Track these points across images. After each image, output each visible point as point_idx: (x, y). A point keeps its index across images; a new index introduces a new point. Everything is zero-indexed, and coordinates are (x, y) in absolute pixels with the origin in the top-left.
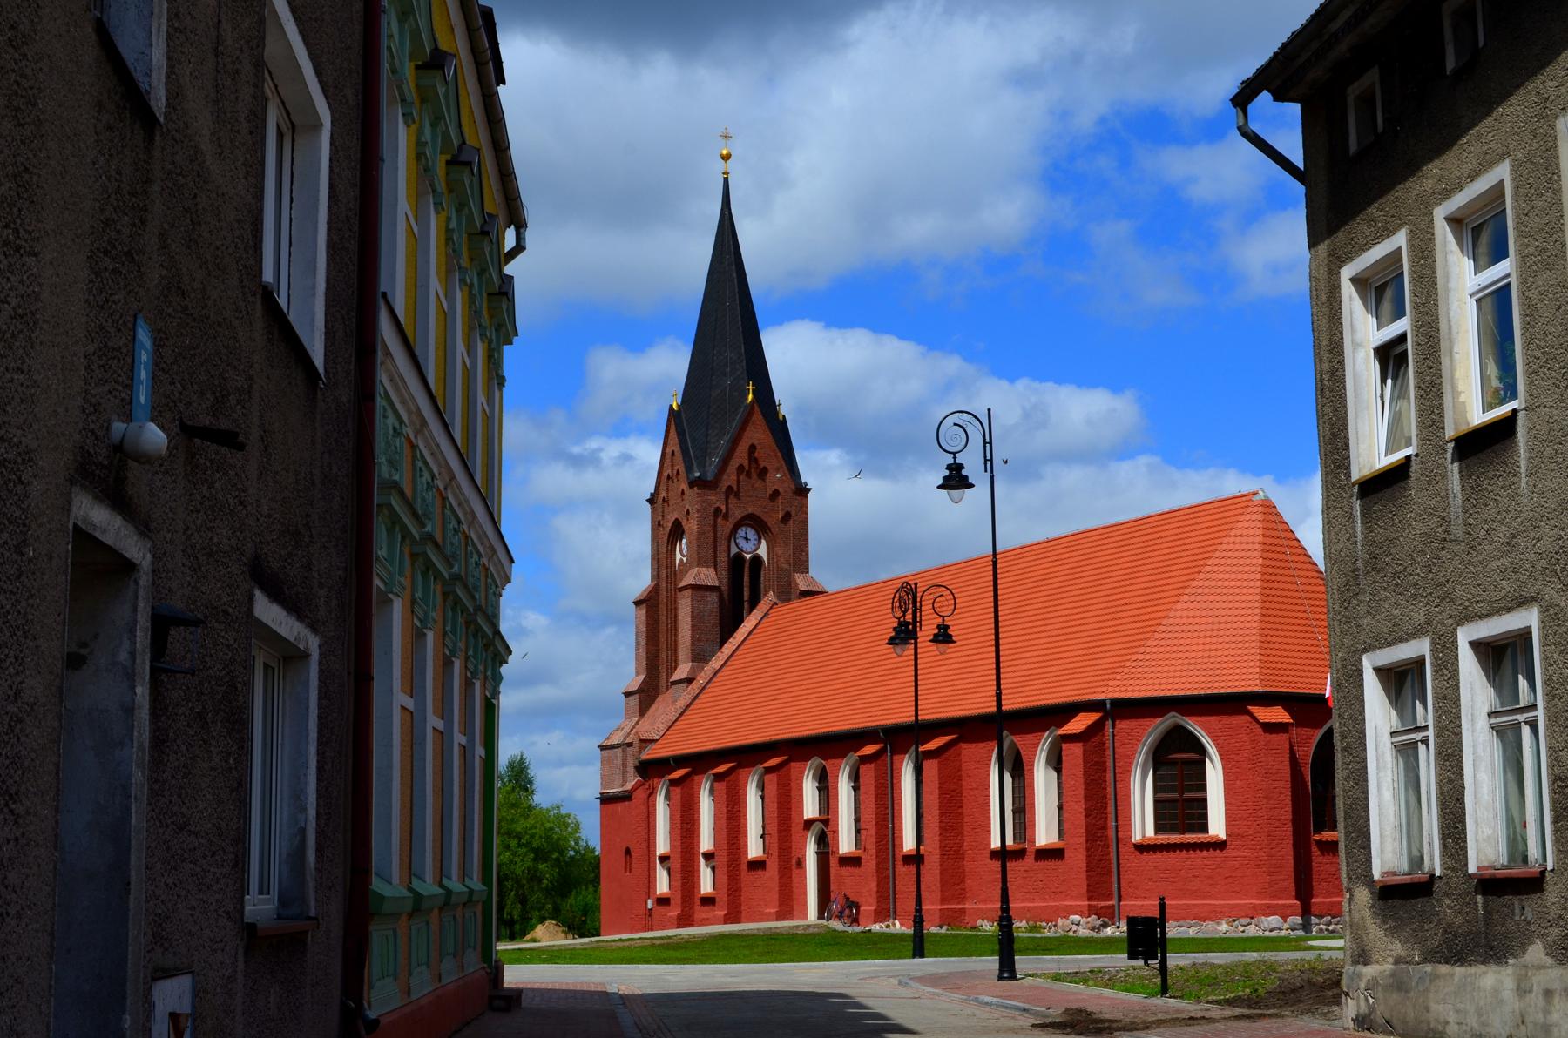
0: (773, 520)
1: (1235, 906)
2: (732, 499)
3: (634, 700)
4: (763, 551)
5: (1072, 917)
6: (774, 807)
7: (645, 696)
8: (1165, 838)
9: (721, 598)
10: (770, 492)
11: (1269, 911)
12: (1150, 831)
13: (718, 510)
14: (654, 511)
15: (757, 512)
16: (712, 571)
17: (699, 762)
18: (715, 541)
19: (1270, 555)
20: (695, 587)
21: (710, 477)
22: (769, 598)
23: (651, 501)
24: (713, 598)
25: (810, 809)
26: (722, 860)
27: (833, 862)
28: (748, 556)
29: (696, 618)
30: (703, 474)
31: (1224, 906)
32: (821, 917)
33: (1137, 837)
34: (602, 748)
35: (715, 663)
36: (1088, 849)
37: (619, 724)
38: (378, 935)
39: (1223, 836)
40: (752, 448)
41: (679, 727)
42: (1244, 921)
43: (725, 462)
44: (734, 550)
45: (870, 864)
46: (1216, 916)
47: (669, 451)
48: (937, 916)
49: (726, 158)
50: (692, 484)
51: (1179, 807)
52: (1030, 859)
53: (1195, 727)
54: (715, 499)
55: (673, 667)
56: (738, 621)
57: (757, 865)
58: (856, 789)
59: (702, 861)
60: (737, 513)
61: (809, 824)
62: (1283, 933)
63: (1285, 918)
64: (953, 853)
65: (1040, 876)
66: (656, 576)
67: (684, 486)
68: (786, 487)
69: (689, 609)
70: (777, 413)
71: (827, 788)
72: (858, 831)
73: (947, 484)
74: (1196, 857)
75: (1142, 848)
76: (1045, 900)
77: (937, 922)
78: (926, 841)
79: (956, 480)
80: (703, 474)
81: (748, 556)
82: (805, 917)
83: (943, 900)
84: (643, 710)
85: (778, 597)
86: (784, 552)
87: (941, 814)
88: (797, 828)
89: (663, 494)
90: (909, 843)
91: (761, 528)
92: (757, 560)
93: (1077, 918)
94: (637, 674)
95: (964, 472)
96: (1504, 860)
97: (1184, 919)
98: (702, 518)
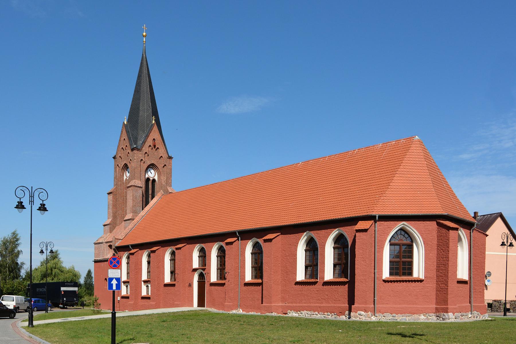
0: (160, 166)
2: (146, 157)
4: (156, 178)
6: (434, 254)
7: (111, 226)
14: (115, 162)
17: (142, 246)
25: (196, 264)
27: (207, 286)
28: (151, 179)
29: (134, 199)
32: (199, 305)
33: (384, 278)
34: (95, 244)
43: (144, 142)
44: (147, 176)
46: (418, 312)
51: (402, 265)
52: (319, 286)
53: (410, 226)
56: (147, 203)
60: (149, 163)
61: (195, 270)
65: (327, 293)
66: (116, 184)
67: (129, 151)
79: (20, 206)
81: (151, 179)
82: (192, 305)
86: (164, 178)
92: (154, 180)
94: (108, 218)
96: (304, 279)
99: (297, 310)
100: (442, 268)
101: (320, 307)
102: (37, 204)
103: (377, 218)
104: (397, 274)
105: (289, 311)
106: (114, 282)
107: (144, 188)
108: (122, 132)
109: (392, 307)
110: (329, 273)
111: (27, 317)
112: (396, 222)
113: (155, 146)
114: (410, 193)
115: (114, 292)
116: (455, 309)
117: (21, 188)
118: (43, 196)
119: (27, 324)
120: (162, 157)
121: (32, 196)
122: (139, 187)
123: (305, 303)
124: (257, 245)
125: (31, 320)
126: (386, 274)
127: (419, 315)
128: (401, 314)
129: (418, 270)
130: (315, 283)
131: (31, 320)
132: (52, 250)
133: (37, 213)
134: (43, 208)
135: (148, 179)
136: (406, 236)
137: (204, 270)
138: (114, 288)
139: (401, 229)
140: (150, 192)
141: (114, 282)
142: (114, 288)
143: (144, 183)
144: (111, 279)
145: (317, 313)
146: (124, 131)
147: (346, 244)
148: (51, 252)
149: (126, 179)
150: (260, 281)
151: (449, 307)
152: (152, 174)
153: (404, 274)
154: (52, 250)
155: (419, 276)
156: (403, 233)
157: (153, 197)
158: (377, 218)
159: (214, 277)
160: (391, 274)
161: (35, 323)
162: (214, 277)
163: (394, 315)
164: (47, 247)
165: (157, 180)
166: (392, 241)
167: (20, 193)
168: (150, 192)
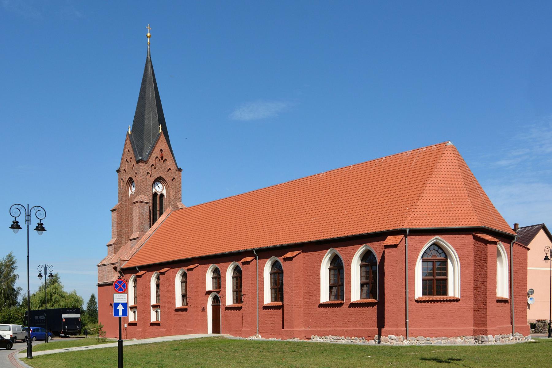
0: (168, 180)
4: (164, 192)
7: (116, 246)
8: (334, 302)
12: (232, 303)
13: (148, 173)
19: (463, 174)
27: (222, 310)
28: (159, 193)
32: (214, 332)
33: (416, 297)
37: (104, 255)
41: (128, 255)
44: (154, 191)
52: (345, 308)
59: (129, 309)
61: (209, 293)
65: (354, 316)
68: (174, 168)
71: (219, 278)
73: (12, 227)
75: (228, 308)
76: (356, 326)
79: (16, 226)
81: (159, 193)
82: (206, 332)
83: (475, 325)
86: (173, 193)
92: (162, 195)
93: (393, 336)
95: (18, 224)
99: (321, 335)
101: (346, 331)
102: (34, 223)
103: (408, 232)
104: (430, 293)
105: (313, 336)
106: (120, 308)
107: (151, 204)
108: (126, 142)
110: (355, 294)
111: (25, 348)
112: (428, 237)
113: (162, 158)
115: (120, 318)
116: (495, 330)
117: (16, 206)
118: (41, 214)
119: (25, 355)
121: (28, 215)
123: (330, 327)
124: (277, 264)
125: (29, 350)
127: (456, 338)
128: (436, 337)
129: (454, 289)
130: (340, 305)
131: (29, 350)
132: (51, 274)
133: (34, 234)
134: (40, 228)
135: (155, 194)
136: (440, 251)
137: (218, 292)
138: (120, 314)
139: (434, 244)
140: (158, 208)
141: (120, 308)
142: (120, 314)
143: (151, 198)
144: (117, 305)
145: (343, 337)
146: (128, 142)
147: (374, 261)
148: (51, 275)
149: (131, 194)
151: (488, 328)
152: (159, 188)
153: (438, 293)
154: (51, 274)
156: (436, 248)
157: (161, 214)
158: (408, 232)
159: (229, 301)
160: (424, 293)
161: (34, 354)
162: (229, 301)
164: (45, 270)
165: (165, 194)
167: (15, 212)
168: (158, 208)
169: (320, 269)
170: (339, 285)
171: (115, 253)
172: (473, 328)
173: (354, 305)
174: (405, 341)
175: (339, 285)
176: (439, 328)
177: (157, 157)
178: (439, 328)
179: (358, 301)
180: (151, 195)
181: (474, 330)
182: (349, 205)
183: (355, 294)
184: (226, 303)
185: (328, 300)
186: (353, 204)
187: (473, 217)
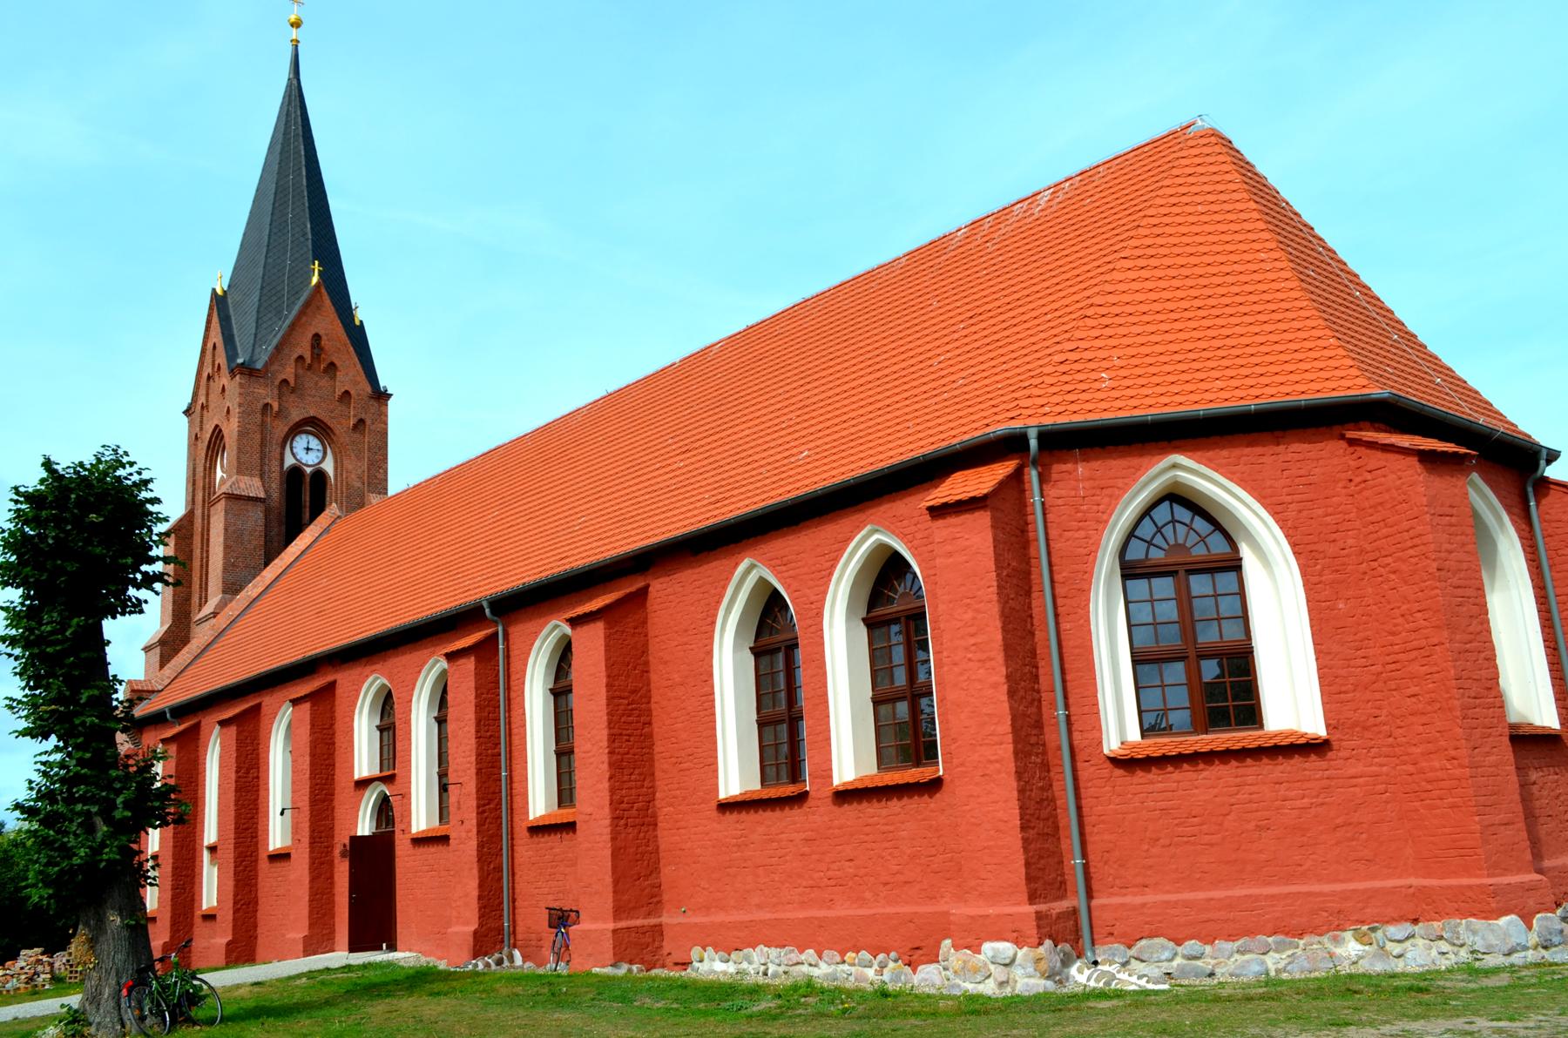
0: (342, 427)
1: (1372, 895)
3: (156, 654)
4: (329, 467)
5: (988, 947)
8: (773, 793)
9: (267, 512)
10: (338, 393)
11: (1487, 906)
12: (1134, 735)
15: (322, 415)
16: (257, 482)
18: (263, 444)
20: (231, 497)
21: (259, 365)
22: (332, 510)
23: (187, 412)
24: (256, 516)
26: (228, 853)
28: (308, 470)
30: (252, 360)
31: (1345, 896)
33: (1112, 744)
35: (252, 590)
36: (1019, 775)
38: (1155, 666)
39: (1313, 724)
40: (317, 337)
42: (1395, 931)
44: (289, 461)
45: (466, 843)
46: (1333, 920)
47: (210, 346)
48: (608, 944)
49: (296, 24)
50: (232, 373)
52: (819, 813)
54: (266, 394)
55: (204, 600)
57: (281, 857)
58: (441, 721)
59: (206, 855)
60: (296, 415)
61: (363, 784)
62: (1531, 956)
63: (1527, 919)
64: (635, 816)
66: (192, 501)
69: (222, 526)
70: (352, 317)
72: (443, 788)
74: (1252, 771)
75: (1127, 763)
77: (609, 956)
78: (581, 794)
80: (252, 360)
81: (308, 470)
84: (164, 661)
85: (341, 509)
86: (357, 468)
87: (612, 738)
88: (343, 790)
89: (202, 399)
90: (539, 801)
91: (316, 426)
92: (319, 475)
93: (1005, 948)
94: (162, 624)
97: (1251, 932)
98: (244, 415)
99: (728, 948)
100: (1415, 668)
103: (1033, 443)
105: (696, 952)
108: (209, 322)
109: (1175, 904)
110: (848, 749)
112: (1135, 461)
114: (1180, 294)
120: (347, 392)
122: (249, 499)
123: (759, 906)
126: (1119, 723)
127: (1337, 941)
128: (1231, 937)
129: (1291, 698)
130: (802, 797)
135: (296, 471)
136: (1200, 524)
137: (388, 779)
145: (810, 953)
146: (215, 319)
150: (790, 790)
152: (307, 452)
155: (995, 686)
158: (1033, 443)
160: (1145, 732)
163: (1192, 946)
166: (1136, 552)
169: (710, 653)
170: (785, 720)
171: (162, 666)
172: (611, 926)
173: (846, 796)
174: (1073, 970)
175: (785, 720)
176: (1238, 892)
177: (301, 358)
178: (1238, 892)
179: (872, 777)
180: (276, 475)
181: (1039, 916)
182: (830, 393)
183: (848, 749)
184: (409, 824)
185: (758, 787)
186: (846, 387)
187: (1239, 206)
